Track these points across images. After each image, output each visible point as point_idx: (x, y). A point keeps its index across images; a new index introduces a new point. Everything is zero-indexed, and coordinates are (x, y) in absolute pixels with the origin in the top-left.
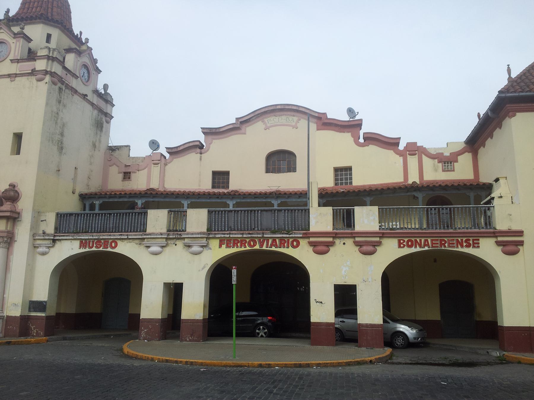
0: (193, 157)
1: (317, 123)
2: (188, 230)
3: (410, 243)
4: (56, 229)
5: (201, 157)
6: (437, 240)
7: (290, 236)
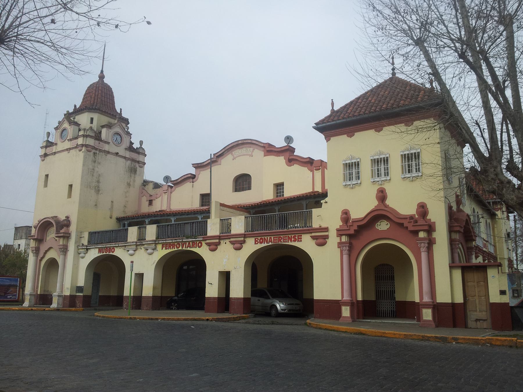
0: (188, 185)
1: (264, 151)
2: (147, 239)
3: (261, 241)
4: (89, 242)
5: (193, 185)
6: (277, 237)
7: (196, 240)
